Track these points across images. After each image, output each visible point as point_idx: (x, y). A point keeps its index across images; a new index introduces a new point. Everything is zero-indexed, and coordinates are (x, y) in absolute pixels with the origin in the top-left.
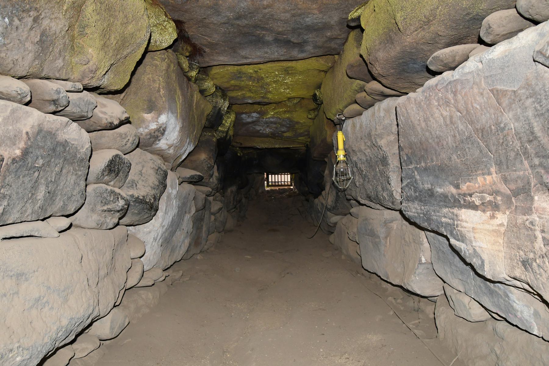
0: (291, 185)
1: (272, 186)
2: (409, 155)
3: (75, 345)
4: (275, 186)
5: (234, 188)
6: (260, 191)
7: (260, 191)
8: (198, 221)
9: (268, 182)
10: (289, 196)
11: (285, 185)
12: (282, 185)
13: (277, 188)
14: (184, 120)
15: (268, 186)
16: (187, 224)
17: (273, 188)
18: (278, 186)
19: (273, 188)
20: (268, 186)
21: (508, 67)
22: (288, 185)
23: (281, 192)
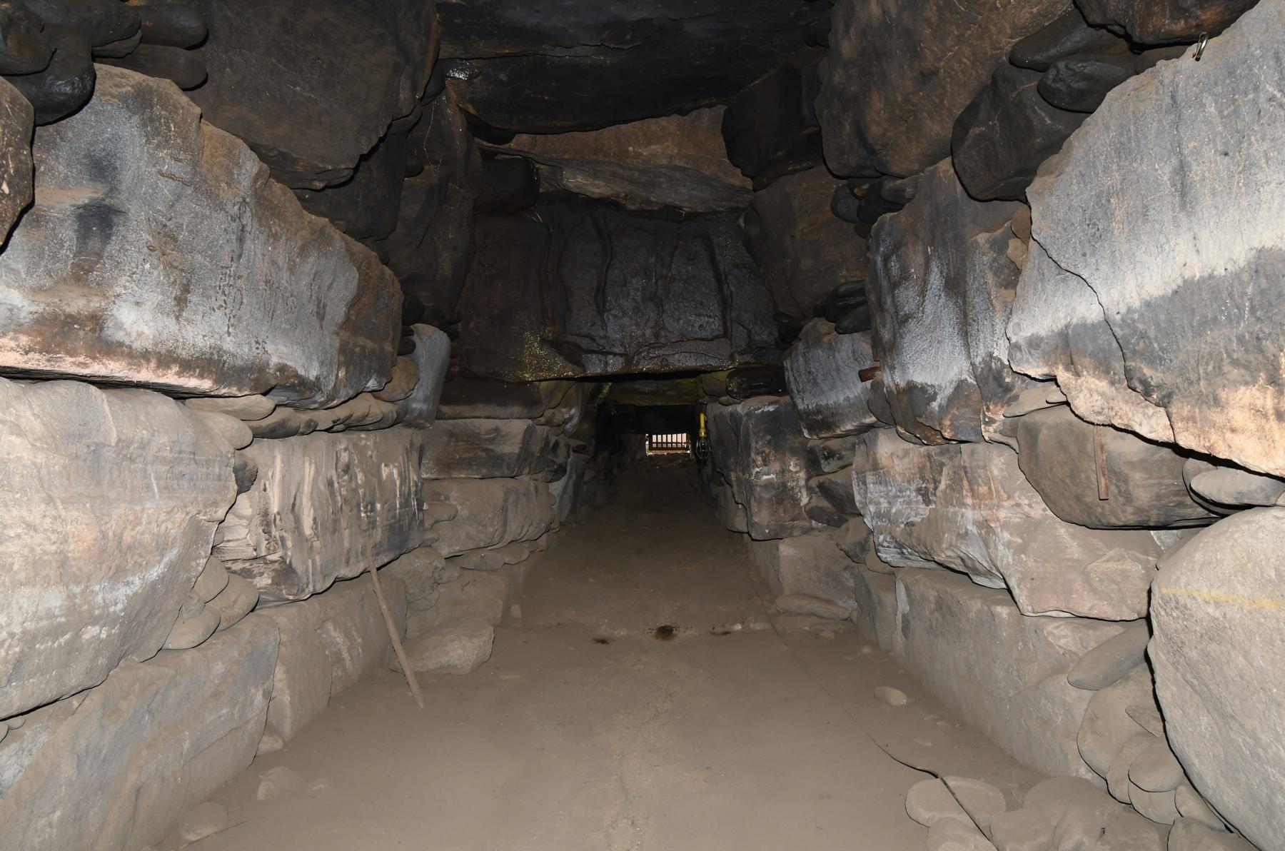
0: (687, 449)
1: (657, 449)
2: (1256, 303)
3: (710, 344)
4: (662, 449)
5: (606, 454)
6: (638, 457)
7: (638, 457)
8: (576, 494)
9: (651, 443)
10: (683, 465)
11: (677, 449)
12: (672, 449)
13: (665, 453)
14: (471, 401)
15: (651, 449)
16: (570, 490)
17: (659, 452)
18: (667, 449)
19: (659, 452)
20: (651, 449)
21: (54, 336)
22: (682, 448)
23: (672, 458)
